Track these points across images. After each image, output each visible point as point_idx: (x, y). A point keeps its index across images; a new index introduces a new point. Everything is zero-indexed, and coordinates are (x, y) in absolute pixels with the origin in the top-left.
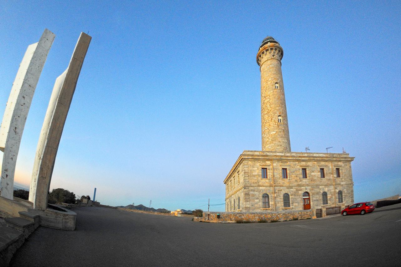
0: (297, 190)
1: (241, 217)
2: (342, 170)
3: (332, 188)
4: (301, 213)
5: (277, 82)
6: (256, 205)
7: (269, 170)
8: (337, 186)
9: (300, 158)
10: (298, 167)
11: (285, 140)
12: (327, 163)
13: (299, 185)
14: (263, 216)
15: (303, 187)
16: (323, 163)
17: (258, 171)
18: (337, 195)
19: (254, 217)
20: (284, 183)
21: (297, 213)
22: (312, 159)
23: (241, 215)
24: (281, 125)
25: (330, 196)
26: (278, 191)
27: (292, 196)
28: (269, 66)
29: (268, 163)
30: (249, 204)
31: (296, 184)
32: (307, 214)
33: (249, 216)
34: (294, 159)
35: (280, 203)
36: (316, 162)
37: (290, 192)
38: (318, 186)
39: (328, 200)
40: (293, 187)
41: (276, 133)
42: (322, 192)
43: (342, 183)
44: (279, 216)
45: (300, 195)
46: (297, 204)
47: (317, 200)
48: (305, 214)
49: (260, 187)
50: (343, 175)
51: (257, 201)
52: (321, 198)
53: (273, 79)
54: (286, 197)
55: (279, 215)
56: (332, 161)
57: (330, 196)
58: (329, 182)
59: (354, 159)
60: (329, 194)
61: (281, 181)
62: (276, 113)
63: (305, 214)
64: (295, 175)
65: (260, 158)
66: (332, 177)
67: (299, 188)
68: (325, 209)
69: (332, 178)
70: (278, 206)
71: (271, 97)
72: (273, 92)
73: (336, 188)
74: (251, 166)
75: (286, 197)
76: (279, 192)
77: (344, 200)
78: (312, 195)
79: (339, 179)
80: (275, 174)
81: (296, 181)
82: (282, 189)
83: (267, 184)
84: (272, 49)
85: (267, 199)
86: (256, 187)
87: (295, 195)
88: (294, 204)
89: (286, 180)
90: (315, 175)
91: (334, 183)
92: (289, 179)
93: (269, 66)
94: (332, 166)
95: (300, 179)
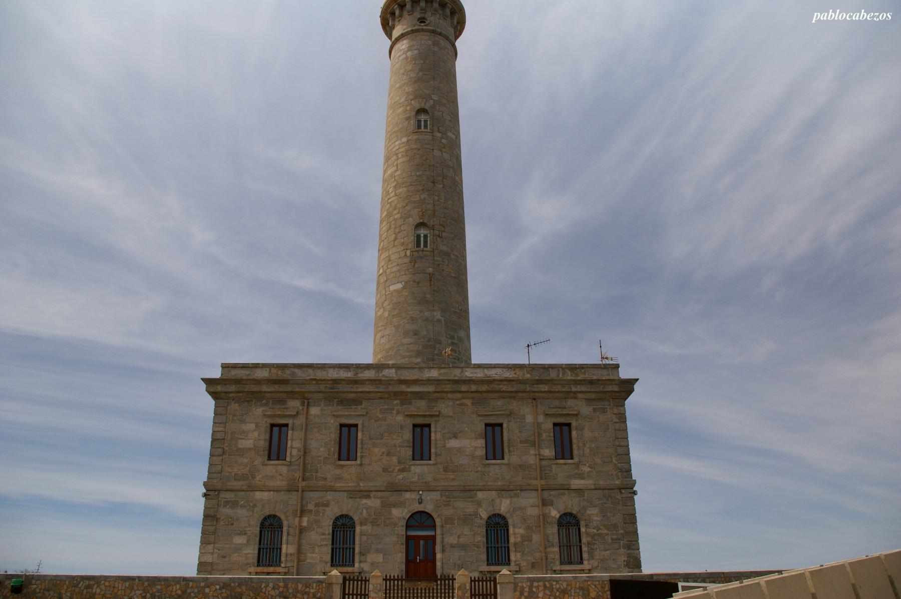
0: (387, 505)
1: (90, 590)
2: (581, 429)
4: (286, 586)
5: (423, 106)
6: (235, 557)
7: (293, 429)
8: (552, 493)
9: (403, 388)
11: (435, 313)
13: (396, 489)
14: (159, 587)
15: (408, 495)
16: (421, 406)
17: (256, 434)
18: (553, 530)
19: (128, 591)
20: (339, 478)
22: (448, 388)
23: (92, 582)
24: (421, 258)
25: (522, 531)
26: (317, 505)
27: (361, 524)
29: (294, 404)
30: (212, 553)
32: (308, 593)
33: (114, 587)
38: (468, 491)
39: (512, 548)
40: (372, 494)
42: (485, 515)
43: (576, 483)
44: (207, 590)
45: (395, 524)
47: (463, 547)
49: (257, 493)
50: (587, 451)
51: (239, 540)
52: (481, 539)
55: (209, 587)
57: (522, 531)
59: (636, 386)
77: (585, 556)
80: (313, 444)
81: (385, 470)
82: (329, 497)
83: (278, 483)
85: (573, 531)
86: (242, 493)
87: (374, 523)
88: (370, 558)
89: (350, 469)
90: (460, 448)
91: (538, 483)
92: (361, 465)
95: (399, 462)
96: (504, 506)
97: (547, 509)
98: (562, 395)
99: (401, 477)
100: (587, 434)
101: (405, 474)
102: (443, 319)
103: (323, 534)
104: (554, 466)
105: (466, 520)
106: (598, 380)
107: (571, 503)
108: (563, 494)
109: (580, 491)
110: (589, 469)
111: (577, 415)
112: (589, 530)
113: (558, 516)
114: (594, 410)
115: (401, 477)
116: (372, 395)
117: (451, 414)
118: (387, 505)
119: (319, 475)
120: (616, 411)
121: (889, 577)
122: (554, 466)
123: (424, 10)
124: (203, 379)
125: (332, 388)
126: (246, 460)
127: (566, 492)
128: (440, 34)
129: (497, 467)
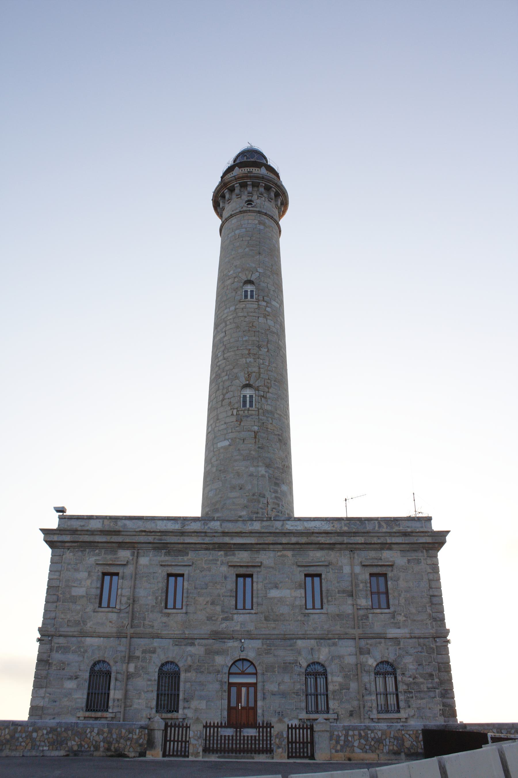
0: (210, 652)
3: (346, 649)
4: (110, 732)
8: (369, 641)
10: (224, 569)
11: (260, 469)
12: (332, 556)
13: (218, 636)
15: (231, 644)
16: (318, 555)
17: (89, 582)
21: (96, 730)
22: (270, 539)
25: (340, 679)
28: (233, 234)
29: (124, 554)
30: (43, 698)
31: (207, 629)
32: (130, 739)
34: (207, 540)
35: (143, 695)
36: (289, 549)
37: (185, 656)
38: (288, 639)
40: (197, 642)
41: (230, 445)
43: (393, 632)
44: (35, 735)
46: (204, 702)
47: (283, 695)
48: (121, 737)
51: (70, 685)
53: (239, 270)
54: (169, 679)
56: (352, 548)
58: (338, 627)
59: (448, 538)
60: (332, 674)
61: (156, 620)
62: (237, 377)
63: (121, 737)
64: (208, 599)
66: (351, 607)
67: (217, 646)
68: (200, 727)
69: (349, 609)
70: (135, 706)
71: (228, 327)
72: (235, 309)
73: (361, 651)
74: (70, 567)
75: (169, 679)
76: (148, 656)
78: (263, 674)
79: (383, 616)
81: (209, 619)
83: (109, 629)
84: (244, 185)
86: (74, 639)
87: (199, 671)
88: (194, 704)
90: (281, 598)
92: (186, 613)
93: (233, 234)
94: (352, 566)
95: (223, 611)
96: (323, 655)
100: (402, 584)
101: (228, 623)
103: (150, 680)
104: (370, 616)
105: (286, 667)
108: (380, 643)
109: (396, 640)
110: (404, 618)
111: (392, 566)
113: (375, 664)
114: (409, 561)
115: (224, 625)
117: (272, 565)
118: (210, 652)
119: (147, 622)
124: (42, 530)
126: (79, 607)
127: (383, 640)
128: (266, 214)
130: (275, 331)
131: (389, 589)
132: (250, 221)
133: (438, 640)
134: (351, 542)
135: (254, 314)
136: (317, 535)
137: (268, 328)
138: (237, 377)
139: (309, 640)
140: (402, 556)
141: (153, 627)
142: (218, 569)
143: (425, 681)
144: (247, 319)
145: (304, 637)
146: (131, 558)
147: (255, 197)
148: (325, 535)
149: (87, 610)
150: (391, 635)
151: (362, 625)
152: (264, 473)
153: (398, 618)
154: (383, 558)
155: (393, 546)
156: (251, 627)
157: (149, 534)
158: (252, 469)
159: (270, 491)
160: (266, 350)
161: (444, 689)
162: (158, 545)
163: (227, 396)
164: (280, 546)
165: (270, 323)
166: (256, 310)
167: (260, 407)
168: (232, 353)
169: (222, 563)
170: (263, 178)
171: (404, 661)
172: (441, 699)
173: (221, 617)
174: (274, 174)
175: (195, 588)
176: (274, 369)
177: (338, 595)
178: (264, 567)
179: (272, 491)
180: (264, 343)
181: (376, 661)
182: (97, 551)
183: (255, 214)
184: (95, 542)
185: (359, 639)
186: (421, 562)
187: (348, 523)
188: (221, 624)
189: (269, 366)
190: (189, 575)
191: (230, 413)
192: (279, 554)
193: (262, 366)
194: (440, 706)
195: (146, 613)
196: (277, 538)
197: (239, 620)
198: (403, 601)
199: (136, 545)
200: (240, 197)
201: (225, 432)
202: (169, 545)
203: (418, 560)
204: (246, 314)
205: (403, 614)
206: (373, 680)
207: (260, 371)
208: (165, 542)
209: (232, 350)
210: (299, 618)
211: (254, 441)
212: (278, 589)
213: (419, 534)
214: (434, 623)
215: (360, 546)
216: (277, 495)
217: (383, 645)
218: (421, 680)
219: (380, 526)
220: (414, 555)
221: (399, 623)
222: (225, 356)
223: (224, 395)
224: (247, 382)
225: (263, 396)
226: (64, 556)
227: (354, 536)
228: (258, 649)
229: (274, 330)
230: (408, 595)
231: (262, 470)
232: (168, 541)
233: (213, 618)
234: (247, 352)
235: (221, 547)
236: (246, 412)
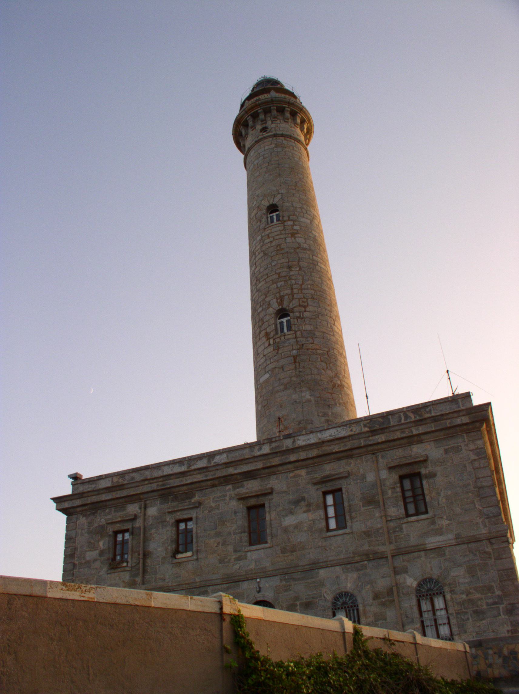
11: (303, 394)
16: (252, 486)
29: (133, 509)
36: (302, 467)
43: (433, 541)
53: (261, 198)
56: (373, 450)
62: (269, 305)
65: (104, 497)
81: (221, 561)
92: (197, 559)
95: (235, 551)
97: (400, 578)
98: (405, 441)
99: (237, 566)
101: (241, 563)
102: (312, 399)
104: (404, 526)
106: (442, 415)
107: (431, 566)
108: (419, 557)
109: (438, 550)
110: (447, 522)
111: (425, 461)
112: (454, 596)
113: (415, 584)
114: (446, 451)
115: (237, 566)
116: (203, 484)
117: (285, 489)
119: (158, 576)
120: (472, 447)
121: (271, 493)
122: (404, 526)
123: (264, 121)
124: (52, 499)
125: (163, 485)
127: (423, 553)
128: (282, 135)
129: (340, 538)
130: (308, 247)
131: (425, 490)
132: (267, 146)
133: (493, 541)
134: (370, 443)
135: (282, 236)
136: (329, 444)
137: (297, 246)
138: (269, 305)
139: (333, 568)
140: (436, 448)
141: (164, 579)
142: (226, 505)
143: (483, 596)
144: (274, 244)
145: (327, 565)
146: (139, 511)
147: (269, 122)
148: (338, 442)
149: (101, 574)
150: (432, 545)
151: (395, 539)
152: (310, 397)
153: (439, 523)
154: (413, 454)
155: (423, 437)
156: (267, 564)
157: (151, 481)
158: (294, 396)
159: (318, 415)
160: (298, 269)
161: (510, 604)
162: (163, 492)
163: (264, 327)
164: (289, 466)
165: (300, 240)
166: (283, 232)
167: (296, 330)
168: (263, 282)
169: (231, 498)
170: (272, 101)
171: (452, 574)
172: (507, 617)
173: (234, 557)
174: (289, 95)
175: (204, 531)
176: (309, 286)
177: (363, 509)
178: (276, 493)
179: (320, 414)
180: (294, 263)
181: (415, 580)
182: (108, 510)
183: (271, 139)
184: (102, 501)
185: (392, 556)
186: (461, 450)
187: (368, 423)
188: (234, 565)
189: (303, 284)
190: (197, 518)
191: (267, 344)
192: (292, 475)
193: (294, 286)
194: (507, 626)
195: (157, 566)
196: (284, 457)
197: (253, 558)
198: (444, 500)
199: (142, 496)
200: (255, 128)
201: (265, 365)
202: (174, 490)
203: (458, 447)
204: (272, 239)
205: (445, 517)
206: (414, 604)
207: (292, 292)
208: (168, 486)
209: (262, 280)
210: (320, 544)
211: (294, 366)
212: (293, 515)
213: (451, 415)
214: (487, 521)
215: (383, 446)
216: (327, 418)
217: (423, 559)
218: (478, 595)
219: (406, 417)
220: (452, 443)
221: (441, 528)
222: (258, 287)
223: (260, 327)
224: (280, 307)
225: (299, 317)
226: (78, 522)
227: (372, 436)
228: (276, 587)
229: (305, 246)
230: (450, 492)
231: (307, 395)
232: (171, 486)
233: (225, 560)
234: (277, 277)
235: (227, 480)
236: (282, 338)
